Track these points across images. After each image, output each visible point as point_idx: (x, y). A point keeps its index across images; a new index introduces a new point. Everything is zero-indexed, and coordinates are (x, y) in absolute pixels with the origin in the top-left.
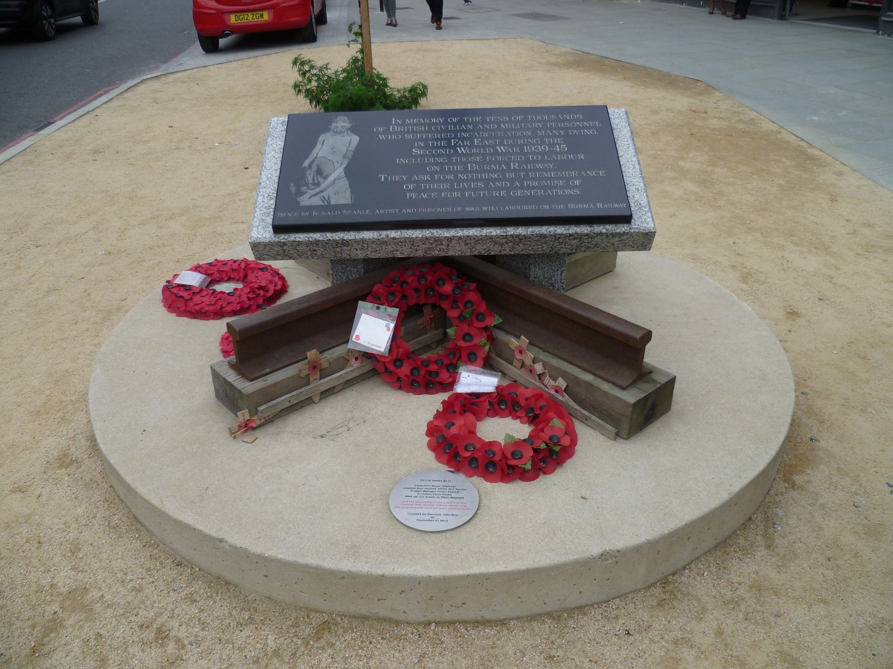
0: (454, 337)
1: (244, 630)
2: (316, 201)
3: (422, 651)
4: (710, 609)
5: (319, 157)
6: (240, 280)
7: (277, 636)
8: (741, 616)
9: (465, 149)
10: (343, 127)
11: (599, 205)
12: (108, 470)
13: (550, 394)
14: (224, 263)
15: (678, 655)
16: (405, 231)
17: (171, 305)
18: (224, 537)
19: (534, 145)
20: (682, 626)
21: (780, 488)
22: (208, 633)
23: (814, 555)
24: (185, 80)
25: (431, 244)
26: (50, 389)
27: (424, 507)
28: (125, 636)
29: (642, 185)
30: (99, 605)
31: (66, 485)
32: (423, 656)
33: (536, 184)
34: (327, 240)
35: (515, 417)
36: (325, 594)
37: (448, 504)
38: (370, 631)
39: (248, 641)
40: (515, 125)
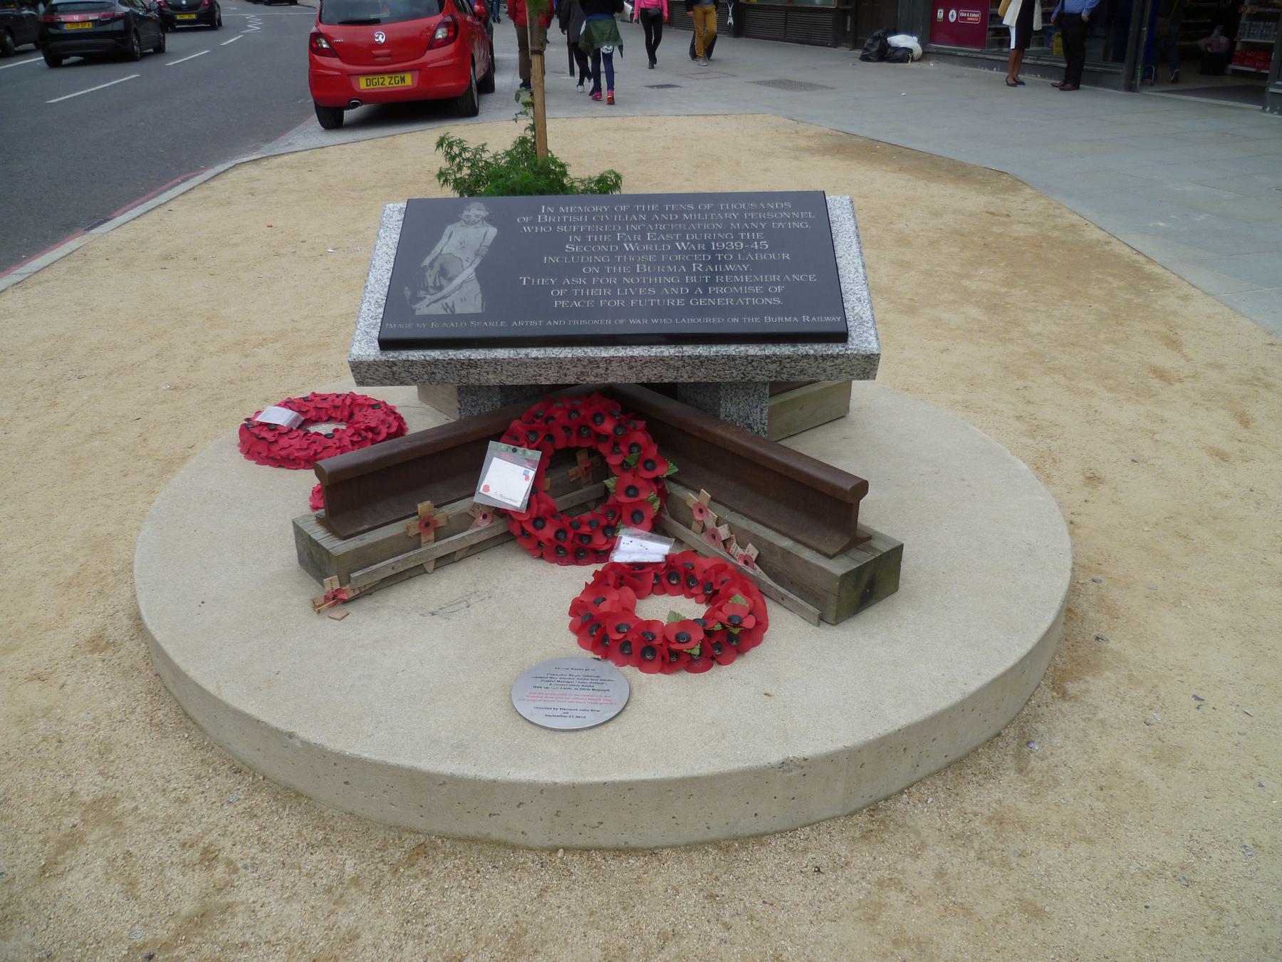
0: (614, 491)
1: (316, 852)
2: (437, 309)
3: (544, 883)
5: (444, 254)
6: (344, 420)
7: (357, 861)
8: (972, 854)
9: (634, 245)
10: (477, 216)
11: (806, 318)
12: (155, 651)
14: (324, 398)
15: (882, 900)
16: (551, 349)
17: (249, 450)
18: (294, 731)
19: (725, 241)
20: (891, 864)
21: (1045, 698)
22: (269, 855)
24: (294, 165)
25: (584, 367)
26: (85, 556)
27: (556, 700)
28: (161, 855)
29: (865, 293)
30: (131, 817)
32: (544, 890)
33: (723, 290)
34: (450, 359)
36: (422, 806)
37: (588, 697)
39: (319, 867)
40: (703, 215)
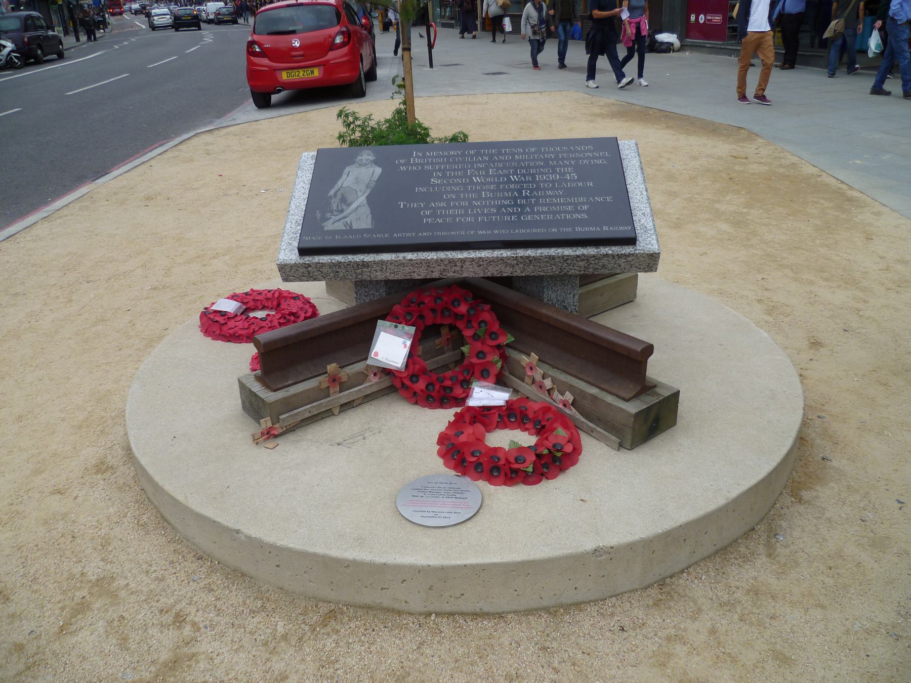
2: (340, 226)
4: (705, 610)
7: (286, 623)
8: (736, 617)
11: (605, 228)
12: (141, 473)
13: (558, 408)
14: (260, 293)
16: (421, 253)
19: (546, 174)
23: (815, 564)
25: (446, 265)
30: (124, 591)
31: (101, 488)
33: (545, 209)
35: (525, 429)
38: (373, 620)
